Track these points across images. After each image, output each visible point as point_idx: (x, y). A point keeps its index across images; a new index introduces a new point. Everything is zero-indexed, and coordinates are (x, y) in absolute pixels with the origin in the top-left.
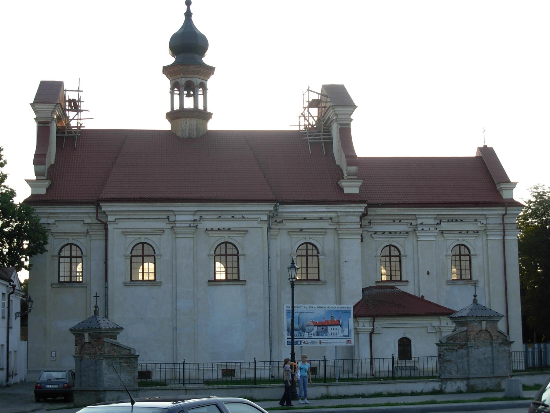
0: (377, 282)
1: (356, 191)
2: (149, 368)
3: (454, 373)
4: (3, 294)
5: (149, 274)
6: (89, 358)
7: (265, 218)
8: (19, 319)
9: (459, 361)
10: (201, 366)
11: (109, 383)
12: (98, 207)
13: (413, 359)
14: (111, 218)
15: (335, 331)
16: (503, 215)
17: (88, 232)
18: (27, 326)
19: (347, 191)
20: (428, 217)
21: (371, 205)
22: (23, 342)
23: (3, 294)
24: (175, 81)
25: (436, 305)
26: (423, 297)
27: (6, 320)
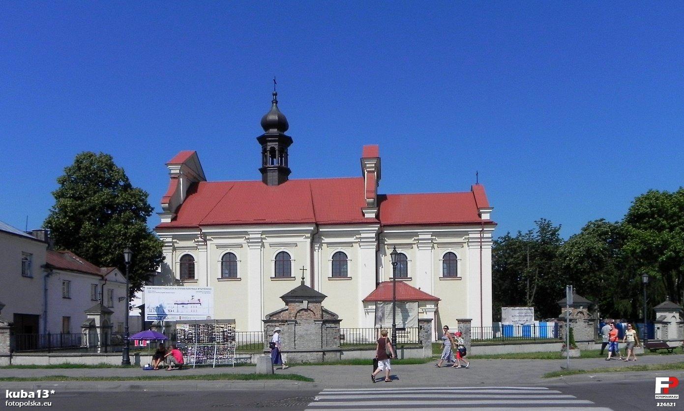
0: (390, 279)
14: (208, 238)
20: (425, 234)
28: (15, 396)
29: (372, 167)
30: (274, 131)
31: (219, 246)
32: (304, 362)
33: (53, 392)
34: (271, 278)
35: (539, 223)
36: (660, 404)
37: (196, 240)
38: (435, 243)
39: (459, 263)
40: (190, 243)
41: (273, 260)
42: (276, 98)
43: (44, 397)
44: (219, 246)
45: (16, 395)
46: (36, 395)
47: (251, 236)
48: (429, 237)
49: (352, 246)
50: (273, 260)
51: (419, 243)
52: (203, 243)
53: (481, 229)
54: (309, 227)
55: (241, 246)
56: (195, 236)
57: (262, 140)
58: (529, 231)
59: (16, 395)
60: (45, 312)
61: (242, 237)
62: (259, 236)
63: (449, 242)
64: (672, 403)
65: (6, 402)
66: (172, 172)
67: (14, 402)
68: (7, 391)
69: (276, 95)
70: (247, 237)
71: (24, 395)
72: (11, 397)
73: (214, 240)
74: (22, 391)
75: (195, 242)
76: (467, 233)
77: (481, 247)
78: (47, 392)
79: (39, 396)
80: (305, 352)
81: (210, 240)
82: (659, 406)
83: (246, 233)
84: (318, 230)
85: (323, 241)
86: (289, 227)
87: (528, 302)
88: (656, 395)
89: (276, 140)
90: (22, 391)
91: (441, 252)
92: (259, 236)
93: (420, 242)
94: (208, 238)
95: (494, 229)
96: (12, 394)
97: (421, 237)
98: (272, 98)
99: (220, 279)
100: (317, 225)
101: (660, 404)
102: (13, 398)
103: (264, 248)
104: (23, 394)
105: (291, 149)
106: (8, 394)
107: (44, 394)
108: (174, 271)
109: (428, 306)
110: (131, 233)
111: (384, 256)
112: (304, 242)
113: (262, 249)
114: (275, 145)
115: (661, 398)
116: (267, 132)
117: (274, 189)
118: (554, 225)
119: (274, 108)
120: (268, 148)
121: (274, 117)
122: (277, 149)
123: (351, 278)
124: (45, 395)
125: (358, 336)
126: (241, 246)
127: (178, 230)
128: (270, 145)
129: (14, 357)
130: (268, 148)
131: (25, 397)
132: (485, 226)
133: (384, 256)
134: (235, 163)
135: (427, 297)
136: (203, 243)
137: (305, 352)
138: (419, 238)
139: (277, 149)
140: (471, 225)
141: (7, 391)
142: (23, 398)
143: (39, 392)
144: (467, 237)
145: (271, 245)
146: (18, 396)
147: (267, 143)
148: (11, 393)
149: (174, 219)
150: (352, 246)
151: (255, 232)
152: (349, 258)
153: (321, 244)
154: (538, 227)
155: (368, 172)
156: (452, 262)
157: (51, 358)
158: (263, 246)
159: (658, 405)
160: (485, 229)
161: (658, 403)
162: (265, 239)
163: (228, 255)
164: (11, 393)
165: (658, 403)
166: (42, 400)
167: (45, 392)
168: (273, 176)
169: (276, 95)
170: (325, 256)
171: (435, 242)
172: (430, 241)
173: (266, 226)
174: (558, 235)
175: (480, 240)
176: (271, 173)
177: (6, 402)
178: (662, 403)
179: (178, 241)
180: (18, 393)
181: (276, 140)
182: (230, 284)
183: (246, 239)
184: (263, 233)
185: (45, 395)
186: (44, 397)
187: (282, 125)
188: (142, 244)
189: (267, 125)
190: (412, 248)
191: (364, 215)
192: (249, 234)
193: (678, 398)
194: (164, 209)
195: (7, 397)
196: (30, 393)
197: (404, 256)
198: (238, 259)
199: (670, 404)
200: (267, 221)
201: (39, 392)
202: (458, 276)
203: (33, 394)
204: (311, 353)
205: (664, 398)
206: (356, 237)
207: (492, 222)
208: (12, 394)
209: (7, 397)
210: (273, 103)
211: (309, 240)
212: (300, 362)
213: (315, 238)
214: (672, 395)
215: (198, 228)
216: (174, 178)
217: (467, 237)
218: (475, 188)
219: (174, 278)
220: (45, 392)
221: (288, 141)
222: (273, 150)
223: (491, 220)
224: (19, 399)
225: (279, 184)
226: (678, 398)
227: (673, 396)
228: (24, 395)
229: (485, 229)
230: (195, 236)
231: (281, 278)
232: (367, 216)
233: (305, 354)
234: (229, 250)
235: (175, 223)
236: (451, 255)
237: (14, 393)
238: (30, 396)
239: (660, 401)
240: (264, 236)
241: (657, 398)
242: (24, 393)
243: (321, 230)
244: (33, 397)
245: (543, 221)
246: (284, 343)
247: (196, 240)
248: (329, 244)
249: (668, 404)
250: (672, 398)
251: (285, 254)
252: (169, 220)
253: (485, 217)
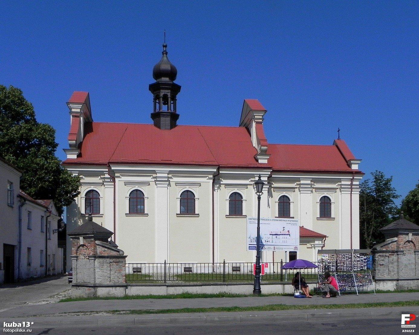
1: (265, 161)
2: (139, 266)
3: (385, 276)
4: (42, 217)
5: (138, 198)
6: (84, 258)
7: (211, 176)
8: (56, 235)
9: (390, 265)
10: (159, 265)
11: (100, 280)
12: (109, 167)
13: (127, 265)
14: (116, 175)
15: (285, 240)
16: (352, 179)
17: (103, 183)
18: (66, 240)
19: (260, 161)
20: (306, 180)
21: (274, 171)
22: (60, 249)
23: (42, 217)
24: (156, 94)
25: (311, 231)
26: (303, 226)
27: (45, 234)
28: (9, 326)
29: (260, 119)
30: (165, 79)
31: (126, 183)
32: (409, 288)
33: (32, 323)
34: (177, 214)
35: (374, 174)
36: (404, 331)
37: (102, 176)
38: (314, 188)
39: (292, 205)
40: (97, 180)
41: (127, 197)
42: (166, 49)
43: (27, 326)
44: (126, 183)
45: (10, 325)
46: (22, 325)
47: (158, 175)
48: (309, 182)
49: (247, 188)
50: (127, 197)
51: (300, 187)
52: (109, 180)
53: (352, 178)
54: (185, 168)
55: (148, 184)
56: (102, 173)
57: (154, 88)
58: (365, 181)
59: (10, 325)
60: (20, 242)
61: (150, 176)
62: (166, 175)
63: (325, 188)
64: (411, 330)
65: (4, 330)
66: (73, 110)
67: (8, 330)
68: (5, 323)
69: (166, 46)
70: (154, 175)
71: (15, 325)
72: (7, 326)
73: (122, 177)
74: (14, 323)
75: (102, 178)
76: (340, 181)
77: (351, 193)
78: (29, 323)
79: (24, 326)
80: (403, 280)
81: (118, 177)
82: (404, 332)
83: (154, 172)
84: (219, 172)
85: (221, 183)
86: (194, 168)
87: (367, 240)
88: (402, 325)
89: (165, 85)
90: (14, 323)
91: (319, 196)
92: (166, 175)
93: (106, 180)
94: (116, 175)
95: (362, 178)
96: (7, 325)
97: (302, 182)
98: (162, 49)
99: (128, 214)
100: (219, 168)
101: (404, 331)
102: (8, 327)
103: (170, 186)
104: (14, 324)
105: (178, 96)
106: (5, 325)
107: (27, 324)
108: (79, 206)
109: (317, 242)
110: (52, 168)
111: (270, 197)
112: (207, 182)
113: (169, 187)
114: (168, 93)
115: (405, 327)
116: (159, 80)
117: (166, 134)
118: (387, 177)
119: (165, 58)
120: (162, 95)
121: (166, 67)
122: (169, 96)
123: (246, 216)
124: (28, 325)
125: (172, 271)
126: (148, 184)
127: (90, 166)
128: (162, 93)
129: (129, 287)
130: (162, 95)
131: (16, 326)
132: (355, 175)
133: (270, 197)
134: (129, 107)
135: (314, 234)
136: (109, 180)
137: (403, 280)
138: (105, 177)
139: (169, 96)
140: (309, 173)
141: (5, 323)
142: (14, 327)
143: (24, 323)
144: (299, 183)
145: (177, 184)
146: (11, 326)
147: (160, 90)
148: (7, 324)
149: (79, 156)
150: (247, 188)
151: (162, 171)
152: (244, 198)
153: (220, 184)
154: (374, 178)
155: (257, 123)
156: (326, 204)
157: (286, 286)
158: (169, 185)
159: (403, 331)
160: (355, 178)
161: (403, 330)
162: (171, 178)
163: (186, 193)
164: (7, 324)
165: (403, 330)
166: (26, 328)
167: (28, 323)
168: (166, 121)
169: (166, 46)
170: (223, 195)
171: (314, 187)
172: (310, 186)
173: (238, 169)
174: (390, 185)
175: (350, 187)
176: (164, 118)
177: (4, 330)
178: (405, 330)
179: (84, 177)
180: (11, 324)
181: (165, 85)
182: (188, 220)
183: (154, 178)
184: (170, 172)
185: (28, 325)
186: (27, 326)
187: (172, 74)
188: (62, 178)
189: (158, 74)
190: (294, 191)
191: (257, 161)
192: (156, 173)
193: (415, 327)
194: (71, 145)
195: (4, 326)
196: (18, 324)
197: (97, 194)
198: (146, 196)
199: (411, 331)
200: (174, 161)
201: (24, 323)
202: (243, 215)
203: (20, 324)
204: (413, 281)
205: (407, 327)
206: (153, 177)
207: (360, 172)
208: (7, 325)
209: (4, 326)
210: (163, 54)
211: (211, 181)
212: (406, 289)
213: (216, 179)
214: (411, 325)
215: (109, 166)
216: (76, 116)
217: (299, 183)
218: (338, 143)
219: (80, 212)
220: (28, 323)
221: (176, 89)
222: (165, 97)
223: (360, 171)
224: (12, 328)
225: (171, 128)
226: (415, 327)
227: (413, 325)
228: (15, 325)
229: (355, 178)
230: (102, 173)
231: (185, 215)
232: (260, 161)
233: (409, 281)
234: (137, 187)
235: (81, 160)
236: (285, 198)
237: (9, 324)
238: (18, 326)
239: (404, 329)
240: (170, 176)
241: (402, 327)
242: (15, 324)
243: (221, 172)
244: (21, 326)
245: (378, 173)
246: (393, 271)
247: (102, 176)
248: (226, 185)
249: (409, 330)
250: (412, 327)
251: (138, 192)
252: (74, 157)
253: (355, 167)
